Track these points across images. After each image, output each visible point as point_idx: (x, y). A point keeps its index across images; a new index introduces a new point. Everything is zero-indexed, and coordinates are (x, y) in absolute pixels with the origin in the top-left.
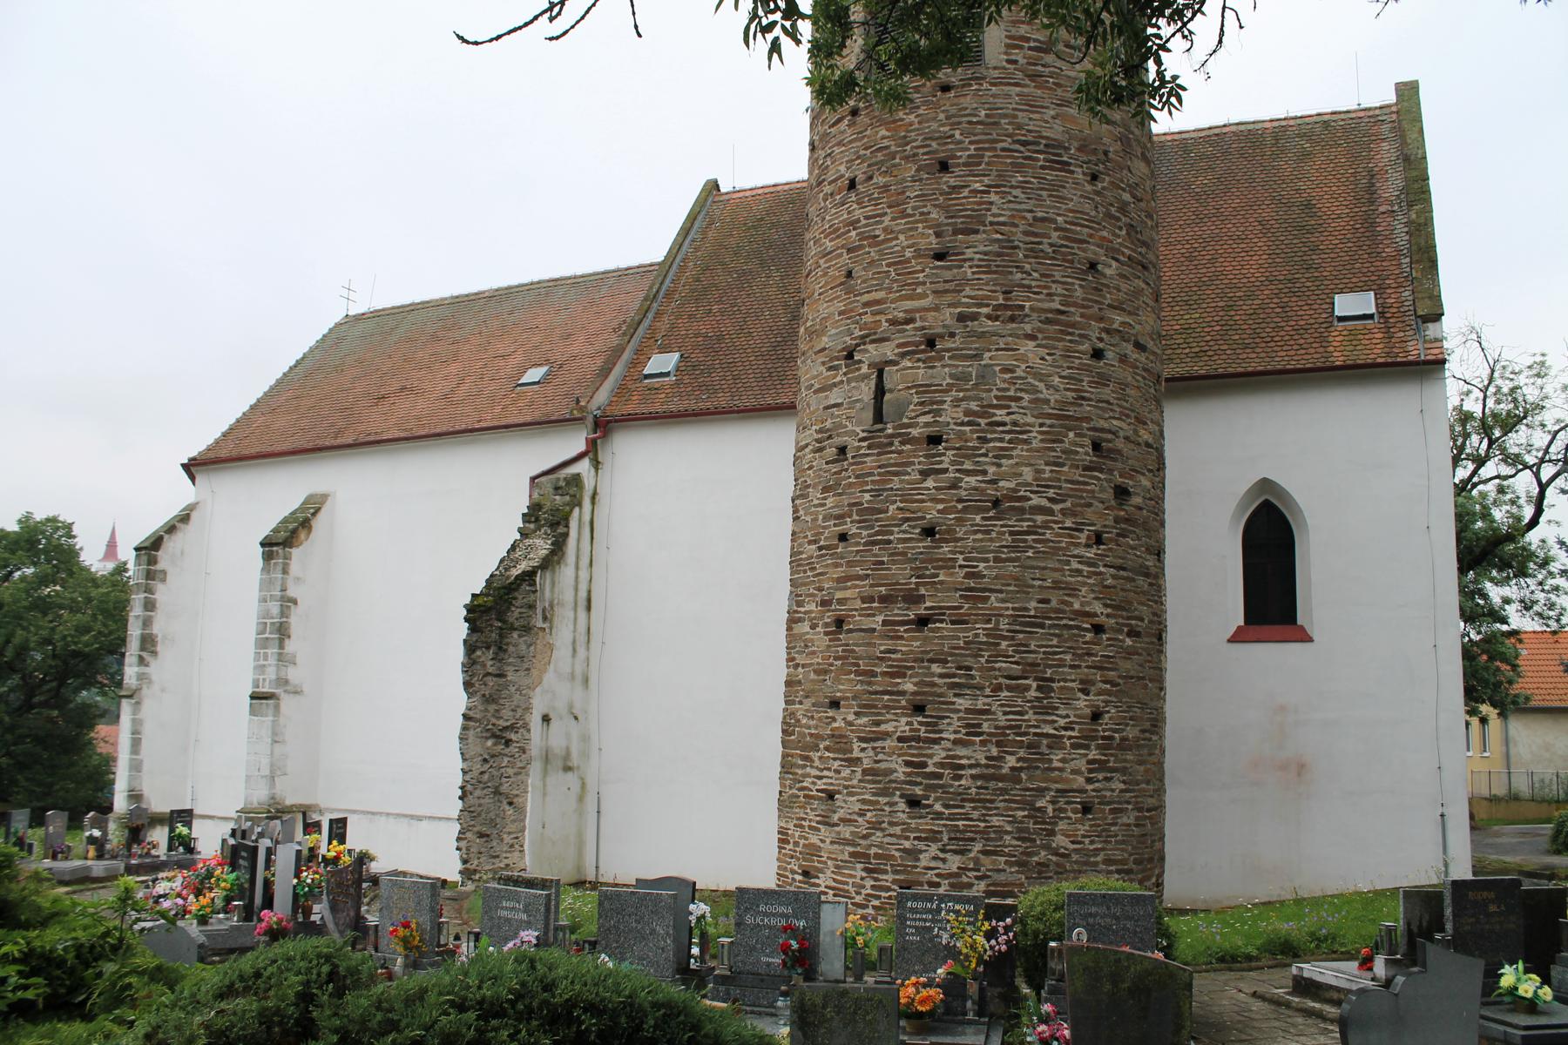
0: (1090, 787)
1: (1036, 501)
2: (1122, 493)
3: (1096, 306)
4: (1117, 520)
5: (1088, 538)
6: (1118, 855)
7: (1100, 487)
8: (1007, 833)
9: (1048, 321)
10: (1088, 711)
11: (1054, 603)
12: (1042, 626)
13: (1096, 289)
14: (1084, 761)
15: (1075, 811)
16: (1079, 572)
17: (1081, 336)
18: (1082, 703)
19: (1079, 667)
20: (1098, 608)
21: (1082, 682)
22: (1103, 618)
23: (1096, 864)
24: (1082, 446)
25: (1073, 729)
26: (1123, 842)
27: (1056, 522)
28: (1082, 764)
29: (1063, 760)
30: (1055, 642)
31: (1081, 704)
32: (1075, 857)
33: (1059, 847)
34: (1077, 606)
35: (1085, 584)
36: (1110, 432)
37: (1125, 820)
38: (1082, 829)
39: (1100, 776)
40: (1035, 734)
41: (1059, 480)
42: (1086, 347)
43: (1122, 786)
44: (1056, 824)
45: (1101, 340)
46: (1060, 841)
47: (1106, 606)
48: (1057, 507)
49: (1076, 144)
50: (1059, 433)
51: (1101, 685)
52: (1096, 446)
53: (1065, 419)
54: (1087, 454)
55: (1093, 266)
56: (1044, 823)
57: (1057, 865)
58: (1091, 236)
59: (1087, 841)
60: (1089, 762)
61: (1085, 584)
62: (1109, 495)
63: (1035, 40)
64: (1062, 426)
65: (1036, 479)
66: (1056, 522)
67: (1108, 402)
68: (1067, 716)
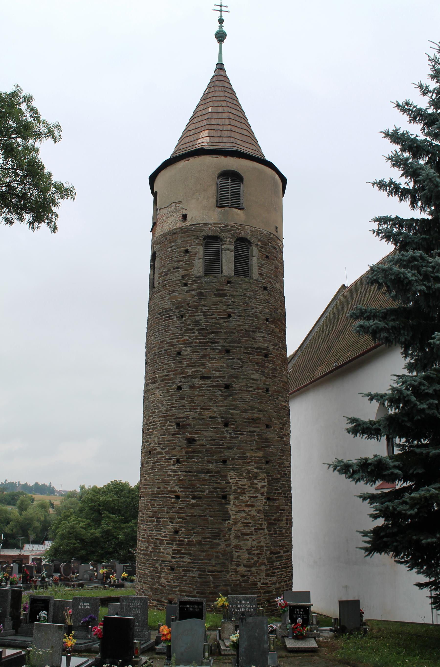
0: (173, 560)
1: (159, 450)
2: (191, 441)
3: (179, 369)
4: (187, 452)
5: (174, 461)
6: (187, 589)
7: (180, 440)
8: (149, 576)
9: (163, 380)
10: (173, 530)
11: (162, 489)
12: (157, 497)
13: (180, 362)
14: (171, 550)
15: (168, 569)
16: (170, 475)
17: (172, 383)
18: (170, 527)
19: (169, 512)
20: (177, 489)
21: (170, 518)
22: (179, 493)
23: (175, 591)
24: (172, 426)
25: (167, 537)
26: (190, 584)
27: (163, 457)
28: (170, 551)
29: (164, 549)
30: (161, 503)
31: (170, 527)
32: (167, 587)
33: (162, 583)
34: (169, 489)
35: (172, 480)
36: (184, 418)
37: (192, 575)
38: (170, 577)
39: (178, 556)
40: (156, 539)
41: (164, 441)
42: (175, 386)
43: (190, 561)
44: (161, 574)
45: (180, 382)
46: (163, 581)
47: (180, 488)
48: (163, 451)
49: (175, 307)
50: (164, 423)
51: (178, 519)
52: (178, 425)
53: (166, 417)
54: (174, 429)
55: (179, 353)
56: (157, 573)
57: (161, 590)
58: (178, 341)
59: (172, 581)
60: (173, 550)
61: (172, 480)
62: (184, 443)
63: (164, 272)
64: (166, 420)
65: (158, 442)
66: (163, 457)
67: (184, 406)
68: (165, 532)
